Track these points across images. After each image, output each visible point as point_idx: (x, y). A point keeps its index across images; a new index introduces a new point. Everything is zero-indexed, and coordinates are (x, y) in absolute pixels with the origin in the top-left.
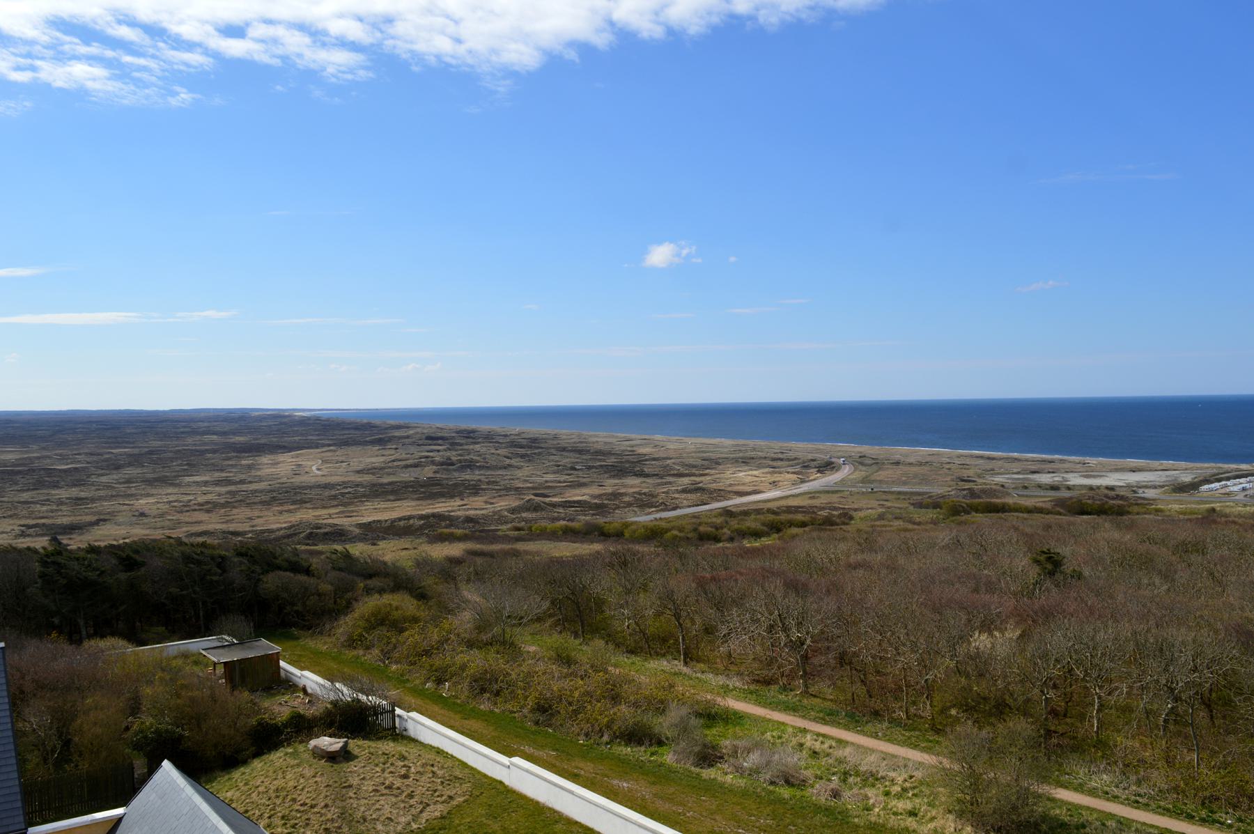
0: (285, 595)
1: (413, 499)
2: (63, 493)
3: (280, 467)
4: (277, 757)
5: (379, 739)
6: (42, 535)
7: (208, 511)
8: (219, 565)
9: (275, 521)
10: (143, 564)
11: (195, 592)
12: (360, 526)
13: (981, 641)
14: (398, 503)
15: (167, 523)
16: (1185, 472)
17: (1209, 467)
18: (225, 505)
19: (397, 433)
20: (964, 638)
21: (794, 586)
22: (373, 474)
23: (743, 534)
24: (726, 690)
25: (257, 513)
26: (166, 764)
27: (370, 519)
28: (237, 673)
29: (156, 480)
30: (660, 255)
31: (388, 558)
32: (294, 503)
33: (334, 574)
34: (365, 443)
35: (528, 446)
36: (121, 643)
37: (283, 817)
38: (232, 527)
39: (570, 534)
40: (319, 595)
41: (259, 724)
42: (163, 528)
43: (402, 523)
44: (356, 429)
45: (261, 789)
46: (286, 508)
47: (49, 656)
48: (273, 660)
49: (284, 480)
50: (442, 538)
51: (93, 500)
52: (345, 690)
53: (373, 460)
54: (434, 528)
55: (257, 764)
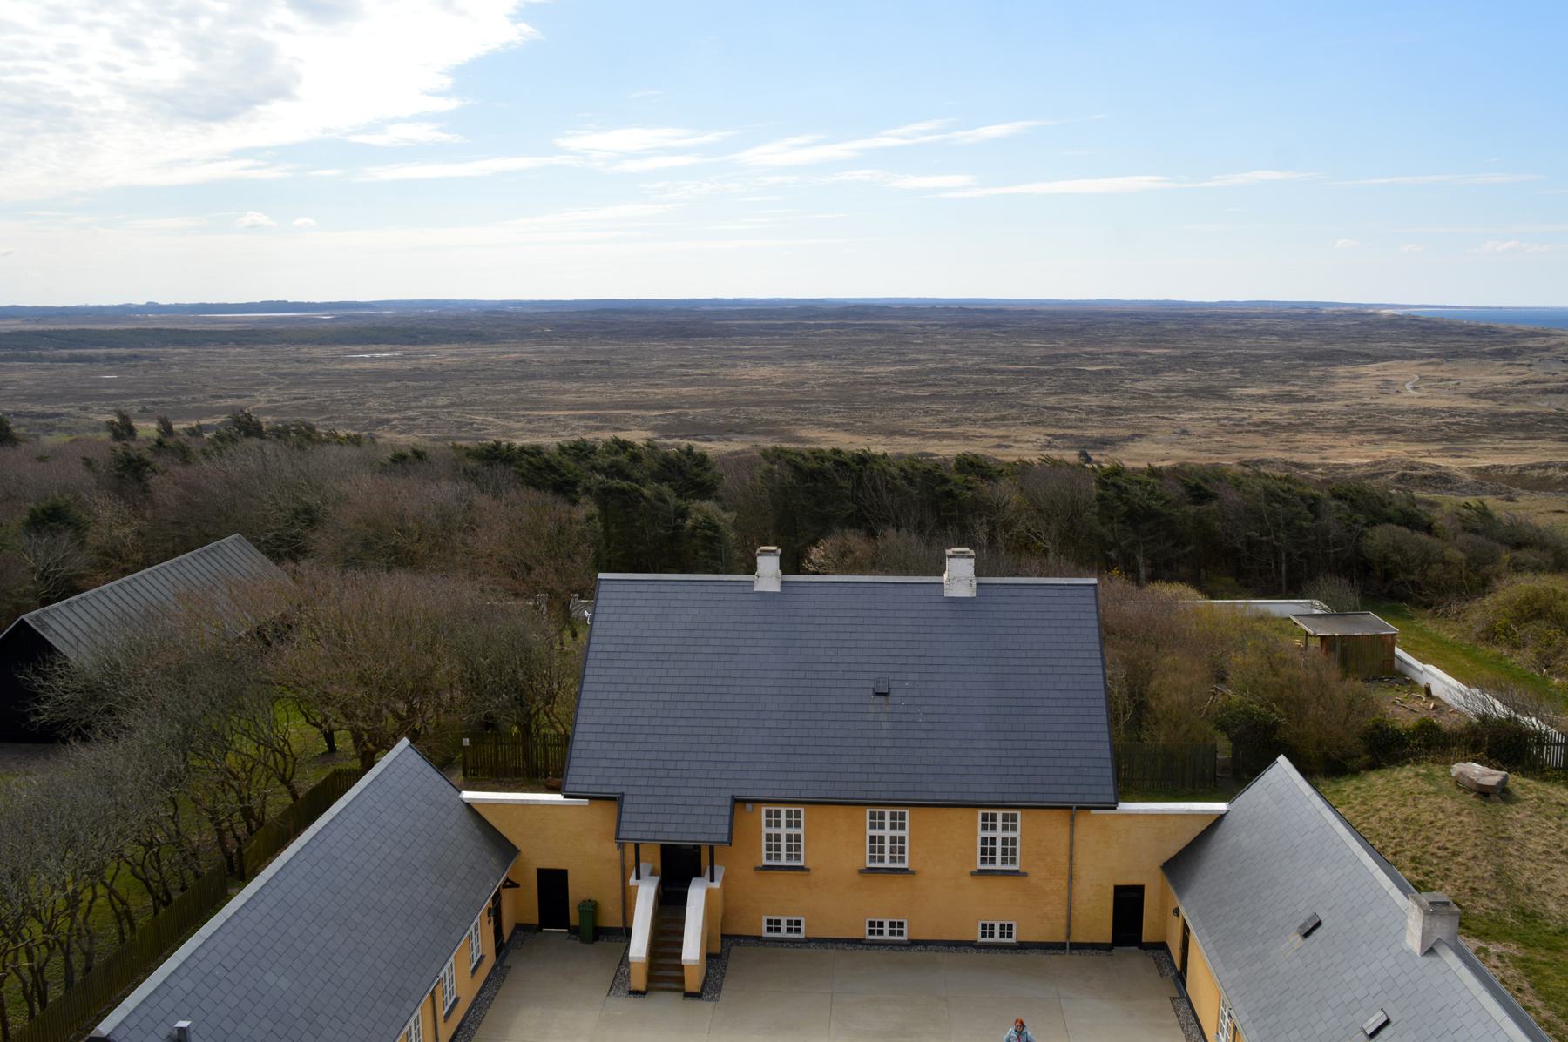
0: (1397, 558)
1: (1554, 440)
2: (1093, 401)
4: (1405, 776)
5: (1546, 780)
6: (1071, 448)
7: (1266, 434)
8: (1310, 508)
9: (1355, 456)
10: (1214, 497)
11: (1277, 538)
12: (1473, 470)
14: (1531, 444)
15: (1214, 445)
18: (1289, 427)
19: (1530, 343)
22: (1494, 399)
25: (1329, 442)
26: (1282, 759)
27: (1488, 463)
28: (1343, 651)
29: (1201, 390)
31: (1542, 521)
32: (1380, 431)
33: (1463, 538)
34: (1482, 355)
36: (1192, 592)
37: (1413, 859)
38: (1297, 457)
40: (1444, 563)
41: (1377, 727)
42: (1209, 450)
43: (1535, 473)
44: (1470, 334)
45: (1383, 814)
46: (1369, 437)
48: (1386, 643)
49: (1367, 400)
51: (1127, 410)
52: (1498, 705)
53: (1496, 379)
55: (1376, 779)
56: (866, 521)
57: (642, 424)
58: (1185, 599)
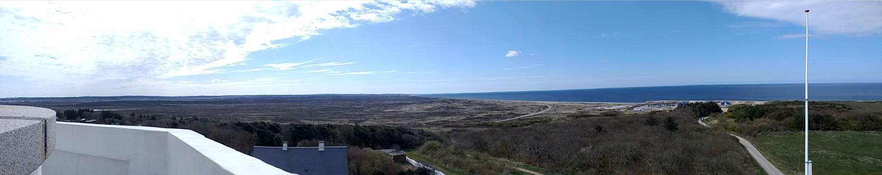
3: (406, 109)
13: (583, 150)
16: (630, 105)
17: (636, 104)
20: (579, 149)
21: (536, 138)
23: (524, 125)
24: (518, 166)
30: (512, 53)
35: (469, 103)
39: (479, 126)
47: (356, 151)
50: (446, 126)
54: (445, 124)
56: (309, 138)
57: (270, 119)
58: (369, 150)
